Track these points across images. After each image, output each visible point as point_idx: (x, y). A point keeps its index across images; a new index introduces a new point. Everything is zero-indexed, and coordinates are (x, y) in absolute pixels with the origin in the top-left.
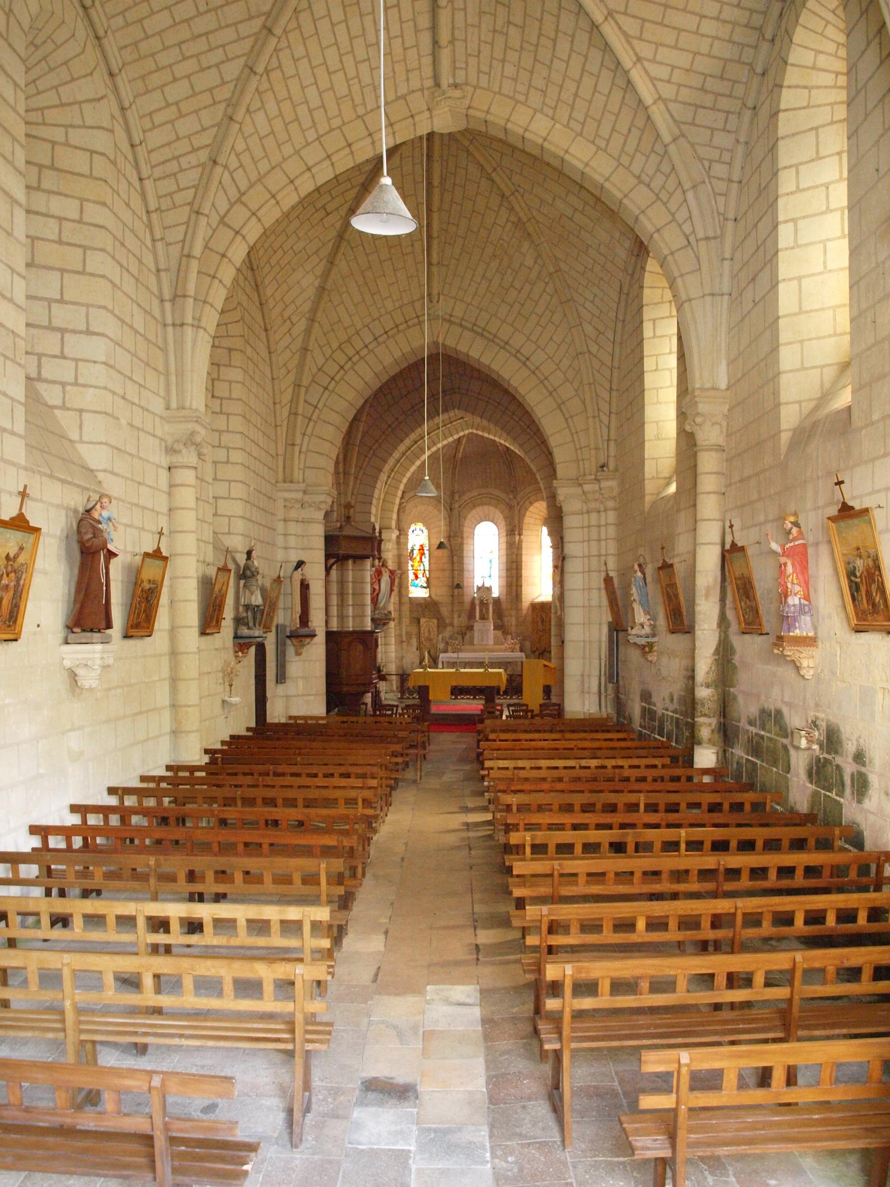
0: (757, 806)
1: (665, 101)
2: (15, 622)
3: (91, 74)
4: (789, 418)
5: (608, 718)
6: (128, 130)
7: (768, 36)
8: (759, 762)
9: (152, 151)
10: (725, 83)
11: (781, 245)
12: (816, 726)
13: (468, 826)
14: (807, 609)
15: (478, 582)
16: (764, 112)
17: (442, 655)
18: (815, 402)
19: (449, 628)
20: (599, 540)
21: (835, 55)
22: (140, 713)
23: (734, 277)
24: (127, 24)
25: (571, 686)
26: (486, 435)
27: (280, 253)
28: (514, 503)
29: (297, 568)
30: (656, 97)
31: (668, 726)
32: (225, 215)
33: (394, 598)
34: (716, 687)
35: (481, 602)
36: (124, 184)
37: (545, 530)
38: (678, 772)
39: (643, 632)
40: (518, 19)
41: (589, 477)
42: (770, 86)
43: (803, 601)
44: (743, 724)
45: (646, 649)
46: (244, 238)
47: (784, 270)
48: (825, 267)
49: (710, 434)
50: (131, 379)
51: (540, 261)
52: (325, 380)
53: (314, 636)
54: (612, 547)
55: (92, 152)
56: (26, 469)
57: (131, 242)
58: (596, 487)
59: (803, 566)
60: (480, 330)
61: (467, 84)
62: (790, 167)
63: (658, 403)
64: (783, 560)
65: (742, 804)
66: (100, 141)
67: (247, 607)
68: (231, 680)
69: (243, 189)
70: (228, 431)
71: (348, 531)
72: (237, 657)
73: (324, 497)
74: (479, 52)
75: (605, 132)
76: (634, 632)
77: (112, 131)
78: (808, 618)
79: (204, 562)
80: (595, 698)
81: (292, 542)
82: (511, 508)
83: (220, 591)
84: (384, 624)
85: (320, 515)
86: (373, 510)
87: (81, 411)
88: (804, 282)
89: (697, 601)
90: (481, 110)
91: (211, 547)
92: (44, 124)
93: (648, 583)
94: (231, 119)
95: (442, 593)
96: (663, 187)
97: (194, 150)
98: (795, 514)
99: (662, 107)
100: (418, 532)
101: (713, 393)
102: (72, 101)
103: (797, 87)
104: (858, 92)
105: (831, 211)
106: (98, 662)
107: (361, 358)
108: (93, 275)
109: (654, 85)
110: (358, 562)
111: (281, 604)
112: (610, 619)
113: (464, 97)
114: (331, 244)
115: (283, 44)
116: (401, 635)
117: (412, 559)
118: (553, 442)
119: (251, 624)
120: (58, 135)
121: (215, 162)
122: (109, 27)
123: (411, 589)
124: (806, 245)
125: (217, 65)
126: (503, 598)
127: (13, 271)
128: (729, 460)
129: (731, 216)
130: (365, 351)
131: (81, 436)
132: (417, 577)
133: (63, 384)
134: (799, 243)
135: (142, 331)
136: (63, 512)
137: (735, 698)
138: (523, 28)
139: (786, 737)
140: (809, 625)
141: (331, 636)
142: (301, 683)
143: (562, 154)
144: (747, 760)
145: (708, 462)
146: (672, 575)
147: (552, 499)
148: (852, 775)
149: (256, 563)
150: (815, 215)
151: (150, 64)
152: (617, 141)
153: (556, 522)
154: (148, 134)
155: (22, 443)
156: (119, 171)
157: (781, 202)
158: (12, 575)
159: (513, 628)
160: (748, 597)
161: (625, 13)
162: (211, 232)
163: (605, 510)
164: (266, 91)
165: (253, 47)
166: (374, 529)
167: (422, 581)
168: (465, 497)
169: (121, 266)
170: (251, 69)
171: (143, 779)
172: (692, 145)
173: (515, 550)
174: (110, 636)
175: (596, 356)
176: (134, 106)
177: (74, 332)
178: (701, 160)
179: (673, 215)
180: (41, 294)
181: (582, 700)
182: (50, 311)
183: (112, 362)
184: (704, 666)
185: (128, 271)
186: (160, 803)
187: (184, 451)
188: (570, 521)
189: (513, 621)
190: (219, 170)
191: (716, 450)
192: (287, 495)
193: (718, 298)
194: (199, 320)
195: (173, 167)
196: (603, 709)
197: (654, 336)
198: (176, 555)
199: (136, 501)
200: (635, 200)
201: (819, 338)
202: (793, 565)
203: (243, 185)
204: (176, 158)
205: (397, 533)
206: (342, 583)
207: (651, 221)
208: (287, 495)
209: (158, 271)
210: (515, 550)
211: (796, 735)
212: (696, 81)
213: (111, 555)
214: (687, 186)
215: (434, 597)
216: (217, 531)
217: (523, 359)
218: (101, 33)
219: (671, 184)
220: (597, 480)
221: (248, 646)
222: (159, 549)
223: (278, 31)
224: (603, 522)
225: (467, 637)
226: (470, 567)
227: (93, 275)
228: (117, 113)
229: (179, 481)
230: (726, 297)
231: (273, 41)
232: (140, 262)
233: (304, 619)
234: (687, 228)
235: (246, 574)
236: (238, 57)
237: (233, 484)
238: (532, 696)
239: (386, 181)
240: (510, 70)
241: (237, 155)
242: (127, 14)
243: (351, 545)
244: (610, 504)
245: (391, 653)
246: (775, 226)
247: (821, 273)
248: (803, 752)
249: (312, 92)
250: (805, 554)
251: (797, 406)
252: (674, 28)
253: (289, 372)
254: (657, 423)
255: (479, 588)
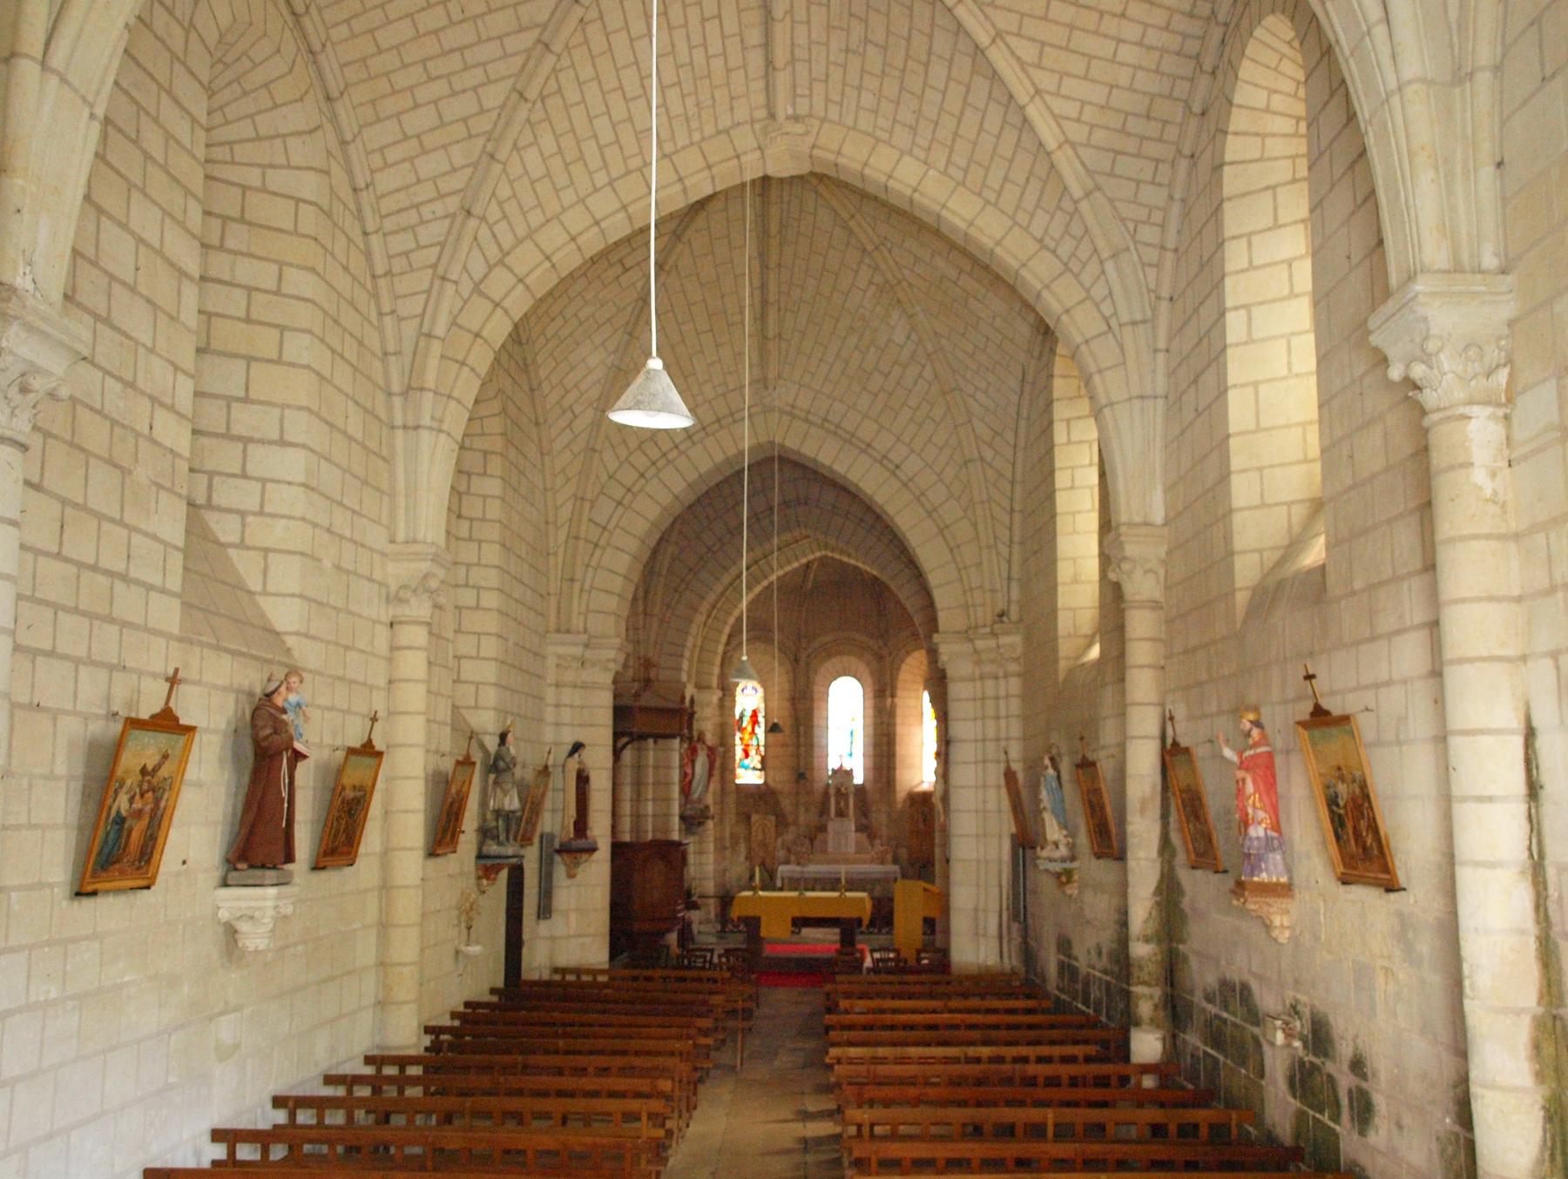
0: (1219, 1131)
1: (1073, 145)
2: (148, 861)
3: (301, 99)
4: (1246, 572)
5: (1014, 972)
6: (349, 171)
7: (1207, 67)
8: (1221, 1058)
9: (383, 196)
10: (1153, 123)
11: (1230, 339)
12: (1297, 1013)
13: (806, 1144)
14: (1276, 843)
15: (833, 764)
16: (1204, 163)
17: (781, 868)
18: (1281, 552)
19: (792, 829)
20: (998, 718)
21: (1295, 95)
22: (332, 978)
23: (1171, 373)
24: (354, 36)
25: (960, 924)
26: (845, 559)
27: (559, 321)
29: (571, 754)
30: (1062, 139)
31: (1095, 993)
32: (482, 281)
33: (714, 786)
34: (1159, 941)
35: (838, 791)
36: (341, 242)
37: (926, 696)
38: (1106, 1069)
39: (1057, 854)
40: (879, 37)
41: (982, 631)
42: (1213, 129)
43: (1270, 833)
44: (1198, 998)
45: (1064, 878)
46: (506, 311)
47: (1234, 374)
48: (1290, 370)
49: (1142, 586)
50: (340, 504)
51: (914, 337)
52: (618, 493)
53: (592, 850)
54: (1015, 729)
55: (298, 201)
56: (180, 640)
57: (350, 319)
58: (992, 643)
59: (1269, 782)
60: (832, 428)
61: (810, 115)
62: (1240, 236)
63: (1075, 532)
64: (1240, 774)
65: (1196, 1126)
66: (309, 186)
67: (498, 813)
68: (470, 919)
69: (506, 247)
70: (478, 564)
71: (648, 700)
72: (479, 885)
73: (609, 656)
74: (827, 75)
75: (995, 180)
76: (1044, 854)
77: (327, 173)
78: (1278, 857)
79: (437, 752)
80: (994, 943)
81: (566, 715)
82: (880, 658)
83: (458, 792)
84: (700, 824)
85: (607, 678)
86: (685, 665)
87: (266, 551)
88: (1262, 388)
89: (1129, 818)
90: (829, 150)
91: (448, 730)
92: (233, 162)
93: (1063, 775)
94: (492, 156)
95: (782, 780)
96: (1073, 254)
97: (441, 197)
98: (1256, 710)
99: (1070, 152)
100: (749, 691)
101: (1144, 530)
102: (272, 132)
103: (1245, 134)
104: (1321, 154)
105: (1297, 296)
106: (270, 913)
107: (669, 462)
108: (293, 365)
109: (1059, 125)
110: (660, 742)
111: (548, 804)
112: (1014, 830)
113: (807, 133)
114: (630, 309)
115: (565, 62)
117: (742, 730)
118: (933, 579)
119: (502, 837)
120: (253, 177)
121: (469, 213)
122: (328, 38)
123: (739, 771)
124: (1263, 340)
125: (475, 89)
126: (868, 786)
127: (176, 368)
128: (1169, 621)
129: (1165, 293)
130: (674, 453)
131: (265, 583)
132: (747, 755)
133: (243, 514)
134: (1255, 336)
135: (359, 436)
136: (231, 698)
137: (1185, 959)
138: (885, 48)
139: (1257, 1024)
140: (1281, 867)
141: (618, 849)
142: (573, 917)
143: (938, 208)
144: (1205, 1053)
145: (1140, 624)
146: (1094, 777)
147: (933, 654)
148: (1350, 1092)
149: (513, 751)
150: (1274, 301)
151: (383, 86)
152: (1010, 196)
153: (939, 685)
154: (378, 176)
155: (176, 604)
156: (335, 225)
157: (1229, 282)
158: (149, 795)
160: (1197, 818)
161: (1019, 35)
162: (460, 304)
163: (1006, 676)
164: (540, 122)
165: (524, 66)
166: (683, 698)
167: (755, 760)
168: (816, 644)
169: (333, 351)
170: (521, 95)
171: (329, 1080)
172: (1111, 201)
173: (885, 719)
174: (291, 874)
175: (990, 465)
176: (358, 140)
177: (262, 442)
178: (1123, 220)
179: (1088, 291)
180: (218, 388)
181: (976, 945)
182: (229, 413)
183: (314, 483)
184: (1141, 911)
185: (342, 357)
186: (350, 1117)
187: (413, 600)
188: (957, 690)
189: (883, 818)
190: (473, 223)
191: (1152, 608)
192: (562, 650)
193: (1150, 403)
194: (441, 421)
195: (412, 217)
196: (1006, 960)
197: (1069, 442)
198: (395, 746)
199: (340, 673)
200: (1037, 272)
201: (1282, 465)
202: (1254, 782)
203: (507, 240)
204: (417, 206)
205: (720, 694)
206: (639, 768)
207: (1059, 298)
208: (562, 650)
209: (385, 354)
210: (885, 719)
211: (1269, 1025)
212: (1115, 121)
213: (298, 756)
214: (1105, 255)
216: (458, 703)
217: (891, 467)
218: (317, 47)
219: (1084, 251)
220: (994, 634)
221: (498, 868)
222: (370, 741)
223: (557, 47)
224: (1002, 693)
225: (817, 843)
227: (293, 365)
228: (335, 149)
229: (403, 642)
230: (1160, 402)
231: (550, 60)
232: (361, 343)
233: (581, 825)
234: (1107, 309)
235: (498, 766)
236: (503, 78)
237: (483, 638)
238: (908, 927)
239: (655, 363)
240: (868, 100)
241: (500, 204)
242: (353, 22)
243: (650, 714)
244: (1013, 668)
245: (705, 866)
246: (1222, 314)
247: (1284, 378)
248: (1280, 1048)
249: (602, 124)
250: (1270, 766)
251: (1256, 556)
252: (1084, 55)
253: (568, 480)
254: (1074, 560)
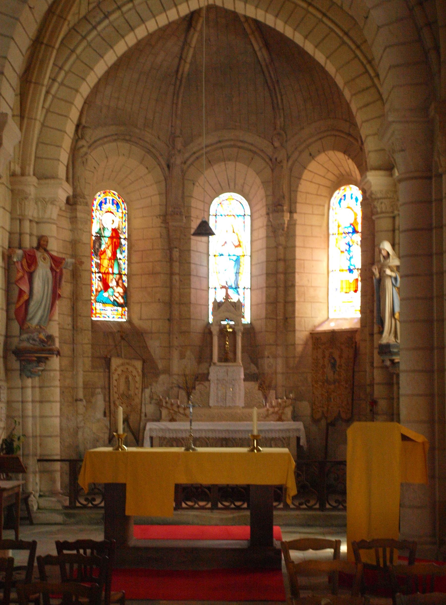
15: (216, 295)
17: (150, 426)
19: (162, 378)
28: (281, 155)
82: (274, 164)
95: (148, 315)
100: (109, 206)
116: (74, 388)
117: (99, 253)
123: (98, 306)
126: (258, 326)
159: (280, 379)
173: (282, 239)
189: (280, 366)
210: (282, 239)
215: (136, 322)
226: (202, 271)
255: (218, 305)
